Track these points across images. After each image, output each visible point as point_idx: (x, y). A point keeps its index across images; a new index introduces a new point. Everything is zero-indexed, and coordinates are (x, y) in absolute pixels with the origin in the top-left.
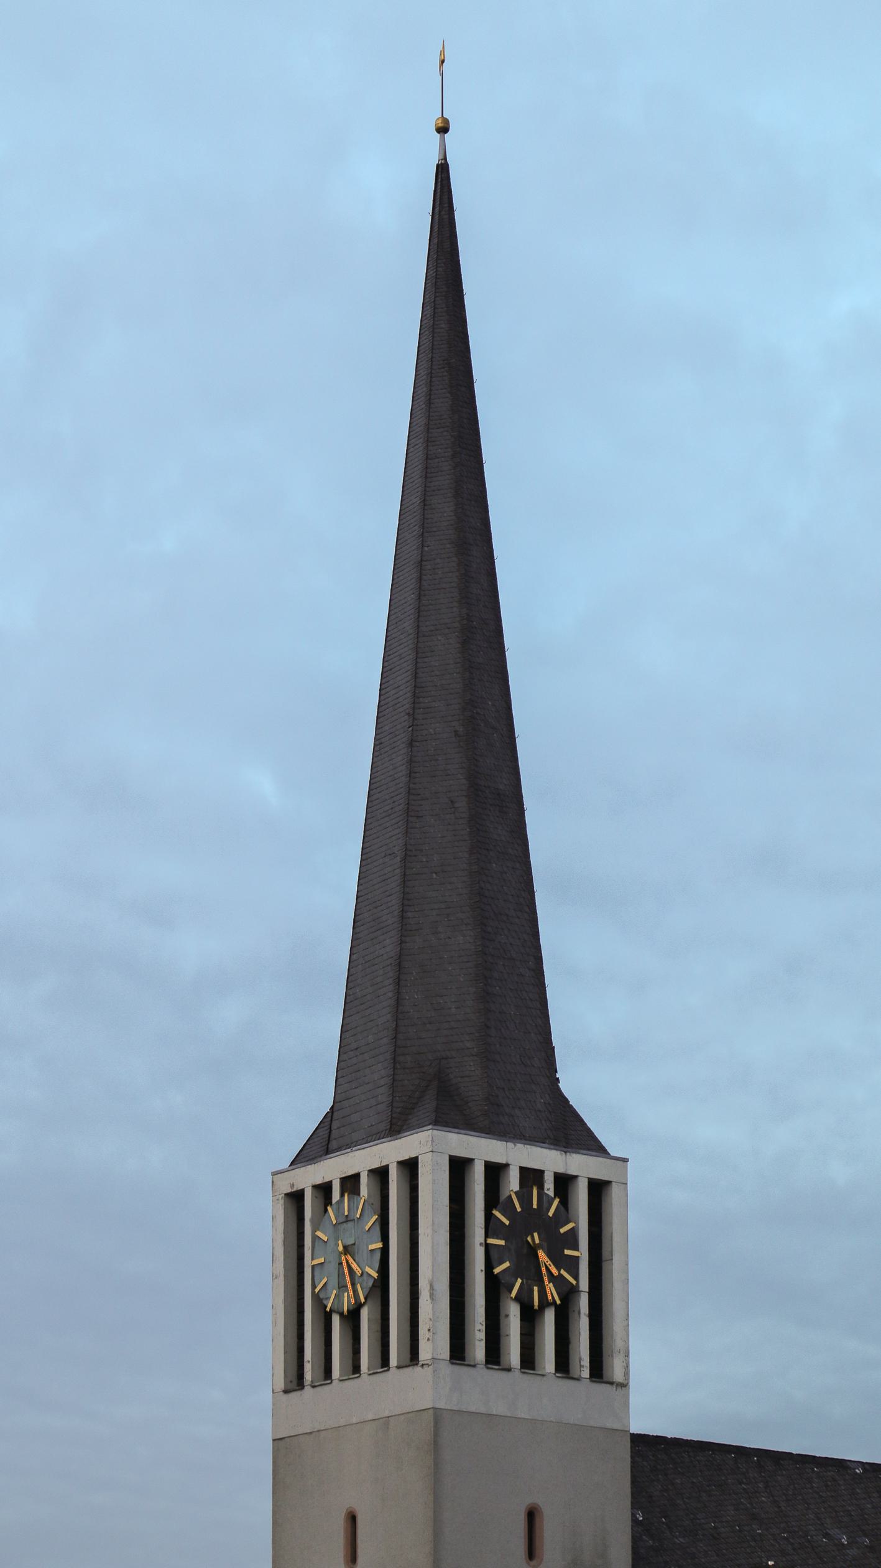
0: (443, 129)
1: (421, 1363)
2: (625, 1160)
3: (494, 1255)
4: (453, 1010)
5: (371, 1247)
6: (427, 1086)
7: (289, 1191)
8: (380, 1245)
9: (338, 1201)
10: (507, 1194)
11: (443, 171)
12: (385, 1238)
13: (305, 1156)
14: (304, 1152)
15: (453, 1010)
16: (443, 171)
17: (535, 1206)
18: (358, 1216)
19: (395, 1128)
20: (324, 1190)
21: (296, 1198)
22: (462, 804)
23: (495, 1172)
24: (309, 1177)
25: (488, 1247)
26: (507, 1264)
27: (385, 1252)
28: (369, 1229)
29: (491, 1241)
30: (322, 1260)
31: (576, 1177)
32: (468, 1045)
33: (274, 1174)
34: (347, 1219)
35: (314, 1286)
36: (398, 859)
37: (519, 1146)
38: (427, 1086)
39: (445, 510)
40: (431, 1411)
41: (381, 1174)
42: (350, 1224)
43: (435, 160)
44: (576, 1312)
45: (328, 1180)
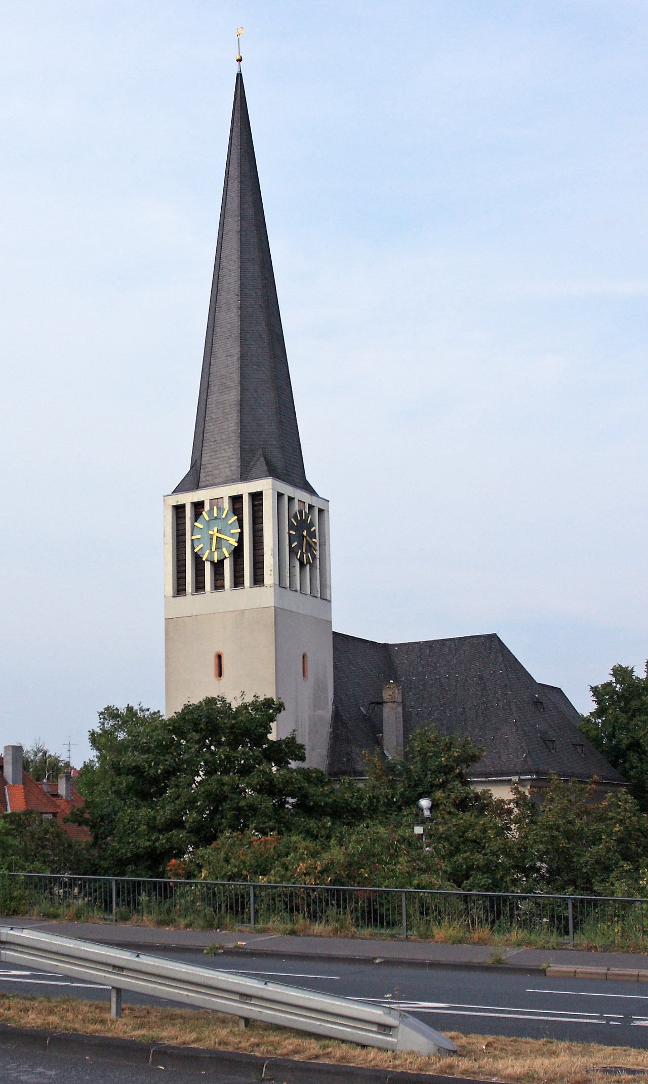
0: (240, 60)
1: (265, 586)
2: (328, 501)
3: (292, 537)
4: (267, 427)
5: (232, 531)
6: (258, 460)
7: (175, 504)
8: (239, 530)
9: (208, 511)
10: (294, 512)
11: (239, 76)
12: (241, 527)
13: (179, 490)
14: (179, 487)
15: (267, 427)
16: (239, 76)
17: (304, 518)
18: (224, 516)
19: (245, 476)
20: (198, 507)
21: (179, 510)
22: (265, 336)
23: (291, 499)
24: (188, 499)
25: (289, 534)
26: (296, 543)
27: (241, 534)
28: (231, 524)
29: (291, 532)
30: (199, 536)
31: (314, 506)
32: (275, 443)
33: (165, 496)
34: (216, 518)
35: (193, 548)
36: (236, 358)
37: (298, 490)
38: (258, 460)
39: (250, 212)
40: (273, 608)
41: (236, 500)
42: (217, 521)
43: (236, 71)
44: (315, 568)
45: (240, 494)
